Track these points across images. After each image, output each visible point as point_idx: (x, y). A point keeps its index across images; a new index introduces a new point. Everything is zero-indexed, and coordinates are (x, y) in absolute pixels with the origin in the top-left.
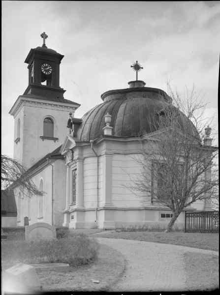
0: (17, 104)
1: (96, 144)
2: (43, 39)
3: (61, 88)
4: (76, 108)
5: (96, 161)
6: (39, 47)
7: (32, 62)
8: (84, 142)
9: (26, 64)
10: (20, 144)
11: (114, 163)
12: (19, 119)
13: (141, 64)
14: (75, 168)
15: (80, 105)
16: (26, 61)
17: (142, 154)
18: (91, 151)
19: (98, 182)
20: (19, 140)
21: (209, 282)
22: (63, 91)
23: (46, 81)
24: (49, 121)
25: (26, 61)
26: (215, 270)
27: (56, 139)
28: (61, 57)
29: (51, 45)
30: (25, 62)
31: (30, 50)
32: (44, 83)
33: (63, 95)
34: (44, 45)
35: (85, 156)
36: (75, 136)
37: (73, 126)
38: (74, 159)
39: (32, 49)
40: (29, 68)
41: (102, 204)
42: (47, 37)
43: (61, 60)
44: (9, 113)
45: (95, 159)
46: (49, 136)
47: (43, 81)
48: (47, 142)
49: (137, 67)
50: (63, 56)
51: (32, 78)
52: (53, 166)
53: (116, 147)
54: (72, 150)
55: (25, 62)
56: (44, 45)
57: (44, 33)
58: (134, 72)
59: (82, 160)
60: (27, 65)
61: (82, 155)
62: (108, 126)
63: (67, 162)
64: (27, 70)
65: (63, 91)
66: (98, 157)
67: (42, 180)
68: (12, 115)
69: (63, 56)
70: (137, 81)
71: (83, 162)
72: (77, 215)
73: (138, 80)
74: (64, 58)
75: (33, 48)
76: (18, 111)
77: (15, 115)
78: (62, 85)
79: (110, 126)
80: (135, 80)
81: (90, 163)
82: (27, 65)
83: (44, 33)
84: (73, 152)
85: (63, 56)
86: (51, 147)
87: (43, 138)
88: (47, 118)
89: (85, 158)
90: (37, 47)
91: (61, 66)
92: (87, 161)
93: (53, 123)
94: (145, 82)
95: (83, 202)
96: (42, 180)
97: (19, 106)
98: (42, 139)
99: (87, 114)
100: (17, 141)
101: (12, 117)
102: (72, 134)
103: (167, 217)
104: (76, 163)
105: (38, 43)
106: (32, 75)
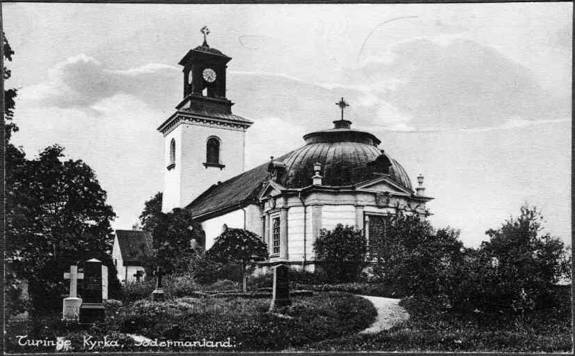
2: (203, 35)
3: (229, 99)
4: (248, 126)
5: (303, 212)
13: (346, 101)
14: (277, 216)
15: (252, 123)
16: (182, 63)
18: (298, 200)
21: (6, 7)
22: (230, 104)
25: (182, 63)
26: (203, 146)
34: (205, 43)
35: (289, 205)
40: (186, 72)
44: (158, 129)
45: (303, 208)
48: (211, 169)
49: (342, 104)
50: (231, 59)
56: (205, 43)
58: (338, 108)
61: (286, 203)
62: (317, 174)
63: (266, 210)
65: (230, 104)
66: (306, 206)
79: (320, 175)
89: (290, 207)
92: (291, 210)
94: (378, 137)
105: (196, 42)
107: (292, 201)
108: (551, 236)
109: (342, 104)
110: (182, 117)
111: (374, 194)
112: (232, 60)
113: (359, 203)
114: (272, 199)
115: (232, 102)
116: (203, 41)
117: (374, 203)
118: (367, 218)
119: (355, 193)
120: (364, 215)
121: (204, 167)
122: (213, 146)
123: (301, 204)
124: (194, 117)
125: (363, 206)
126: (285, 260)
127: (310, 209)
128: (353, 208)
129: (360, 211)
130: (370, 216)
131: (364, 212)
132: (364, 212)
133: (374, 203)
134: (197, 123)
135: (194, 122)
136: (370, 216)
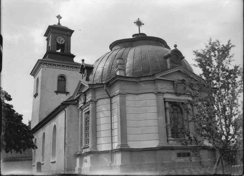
0: (37, 66)
1: (109, 85)
2: (58, 19)
5: (109, 102)
6: (55, 25)
7: (50, 36)
8: (97, 84)
9: (44, 37)
10: (38, 98)
11: (128, 103)
12: (38, 78)
14: (88, 110)
16: (46, 35)
17: (192, 73)
19: (111, 123)
20: (37, 95)
22: (73, 56)
23: (60, 49)
24: (62, 79)
27: (67, 93)
28: (72, 32)
29: (64, 23)
30: (44, 36)
31: (48, 26)
32: (59, 51)
33: (73, 59)
34: (59, 23)
35: (97, 98)
36: (87, 79)
37: (86, 71)
38: (87, 101)
39: (49, 26)
40: (48, 40)
41: (116, 146)
42: (61, 18)
43: (72, 34)
44: (30, 74)
45: (108, 100)
46: (61, 89)
47: (58, 49)
48: (60, 95)
51: (49, 47)
52: (65, 111)
53: (128, 88)
54: (85, 94)
55: (44, 36)
56: (59, 23)
57: (59, 15)
59: (94, 102)
60: (46, 38)
64: (46, 42)
65: (73, 56)
66: (111, 98)
67: (55, 125)
68: (32, 75)
69: (73, 31)
70: (140, 34)
71: (96, 104)
72: (91, 158)
73: (141, 32)
74: (74, 32)
75: (50, 25)
76: (38, 71)
77: (35, 76)
78: (72, 52)
80: (138, 33)
81: (103, 106)
82: (46, 38)
83: (59, 15)
84: (86, 95)
85: (73, 31)
86: (63, 98)
87: (57, 92)
88: (59, 77)
89: (98, 100)
90: (53, 24)
91: (72, 37)
92: (100, 102)
93: (65, 80)
95: (95, 144)
96: (55, 125)
97: (39, 66)
98: (56, 93)
99: (98, 60)
100: (36, 96)
101: (33, 77)
102: (85, 78)
103: (183, 156)
104: (89, 105)
105: (54, 22)
106: (50, 45)
107: (99, 94)
108: (85, 163)
109: (139, 23)
110: (41, 63)
111: (173, 82)
112: (75, 31)
113: (160, 90)
114: (83, 94)
115: (74, 55)
116: (58, 22)
117: (172, 91)
118: (167, 105)
119: (154, 81)
120: (165, 102)
121: (56, 94)
122: (62, 79)
123: (107, 96)
124: (50, 63)
125: (164, 93)
126: (93, 150)
127: (115, 100)
128: (153, 96)
129: (161, 98)
130: (170, 102)
131: (164, 99)
132: (164, 99)
133: (172, 91)
134: (52, 67)
135: (49, 66)
136: (170, 102)
